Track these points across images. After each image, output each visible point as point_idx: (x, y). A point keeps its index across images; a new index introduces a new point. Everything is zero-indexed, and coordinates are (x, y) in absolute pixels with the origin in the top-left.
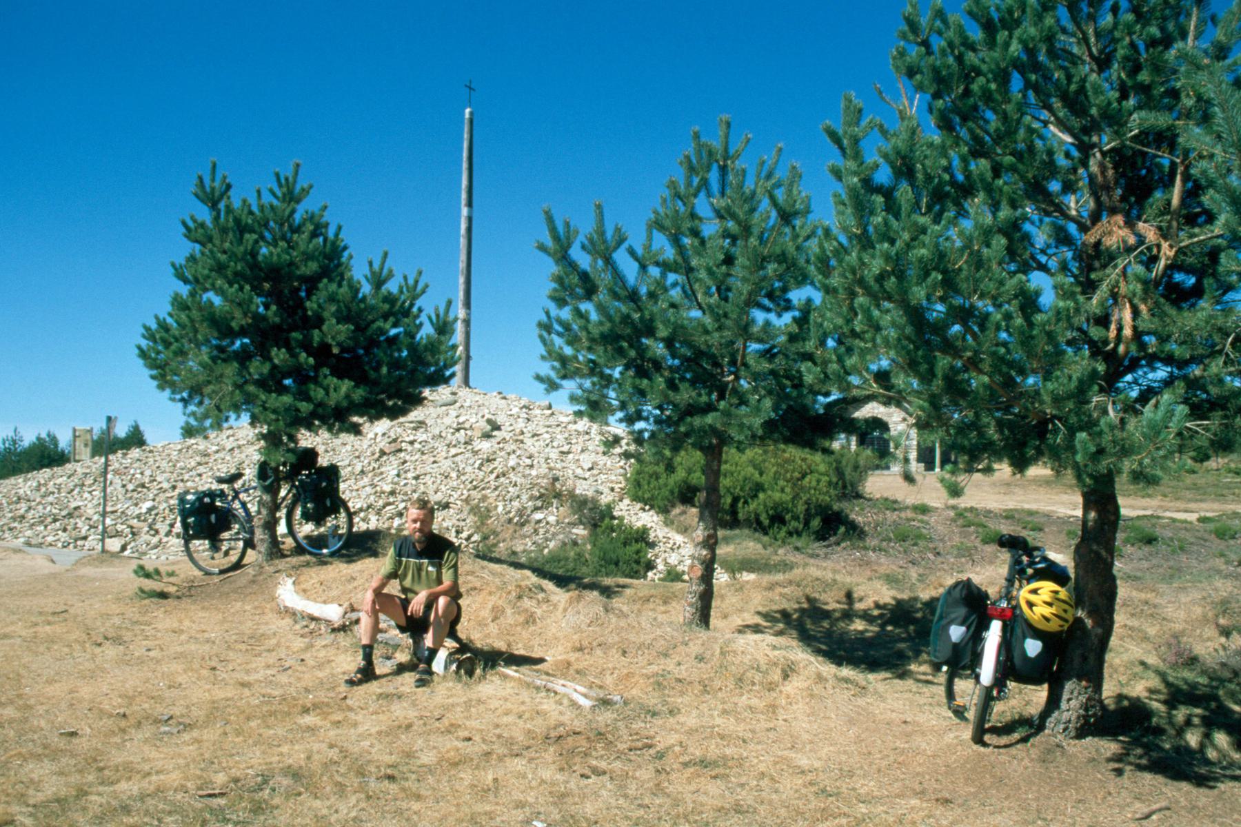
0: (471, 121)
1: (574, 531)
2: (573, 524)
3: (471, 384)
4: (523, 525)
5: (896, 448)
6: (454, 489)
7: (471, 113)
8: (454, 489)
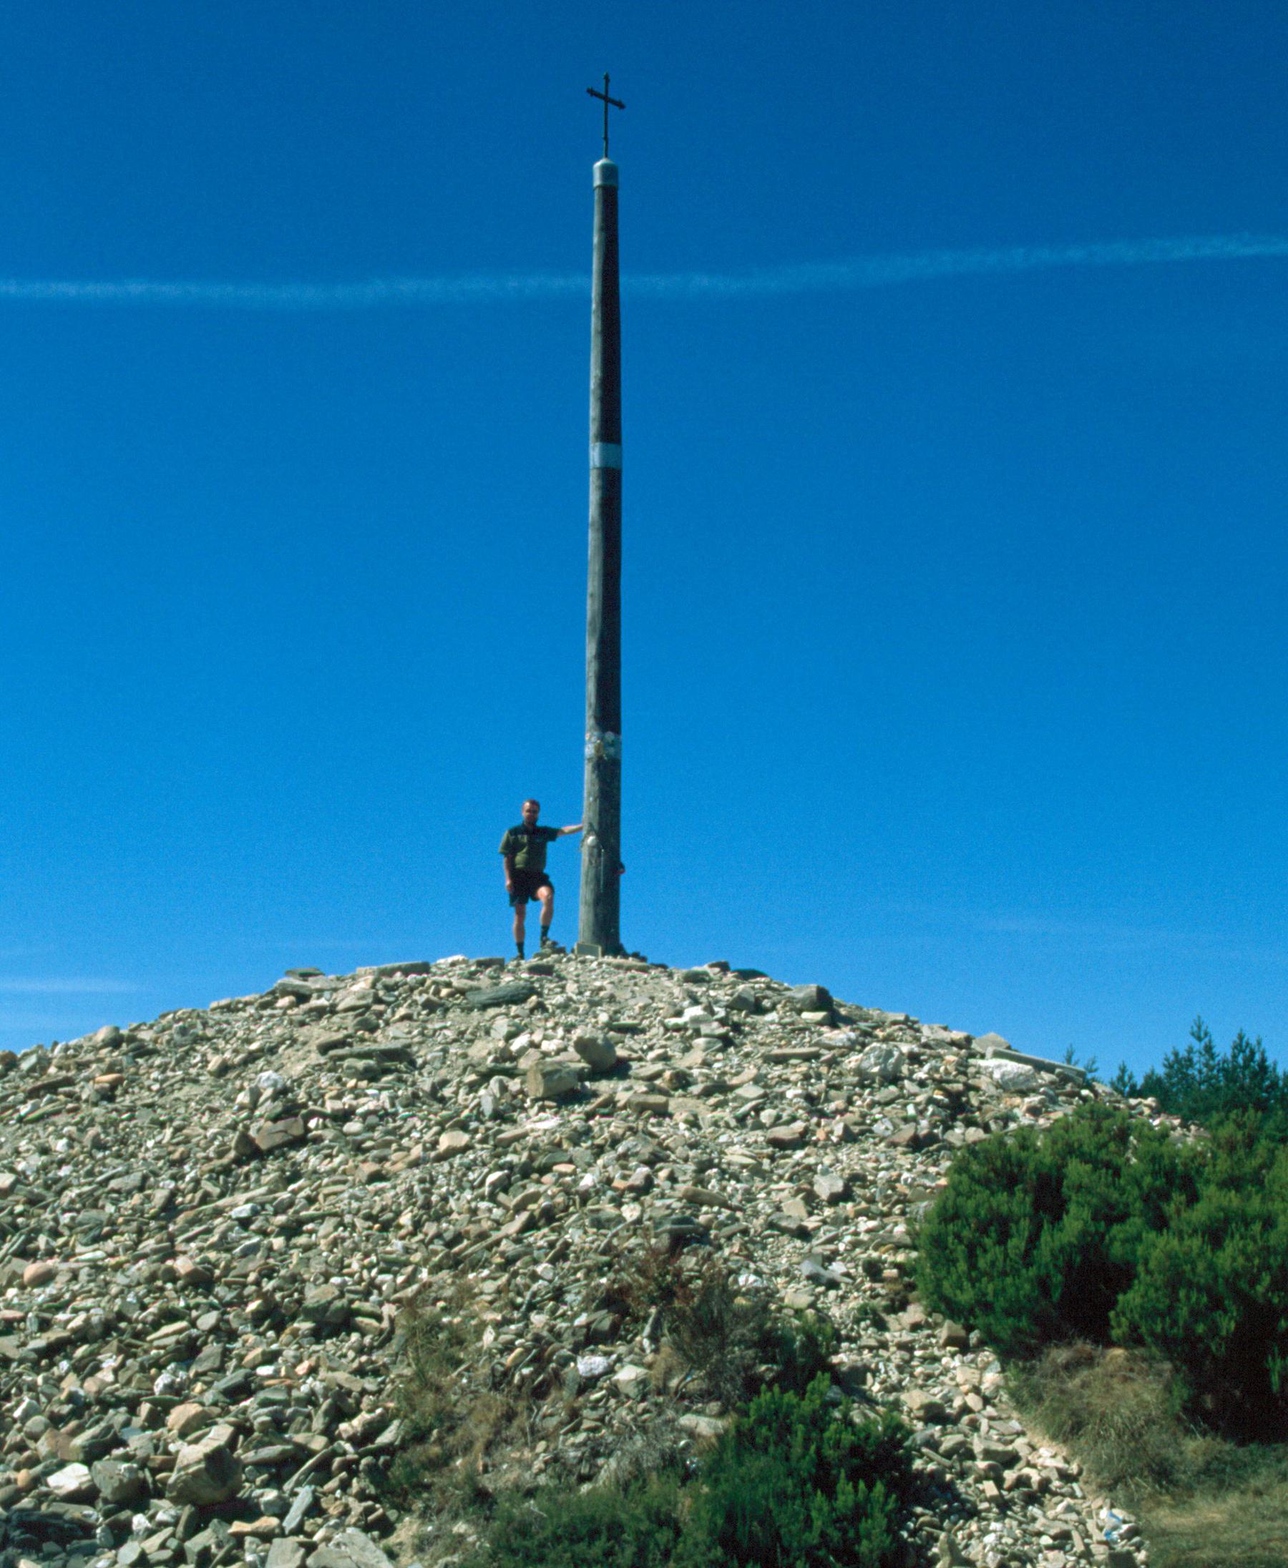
0: (610, 195)
1: (687, 1420)
2: (685, 1400)
3: (627, 939)
4: (540, 1393)
5: (1064, 1423)
6: (390, 1266)
7: (608, 172)
8: (390, 1266)
